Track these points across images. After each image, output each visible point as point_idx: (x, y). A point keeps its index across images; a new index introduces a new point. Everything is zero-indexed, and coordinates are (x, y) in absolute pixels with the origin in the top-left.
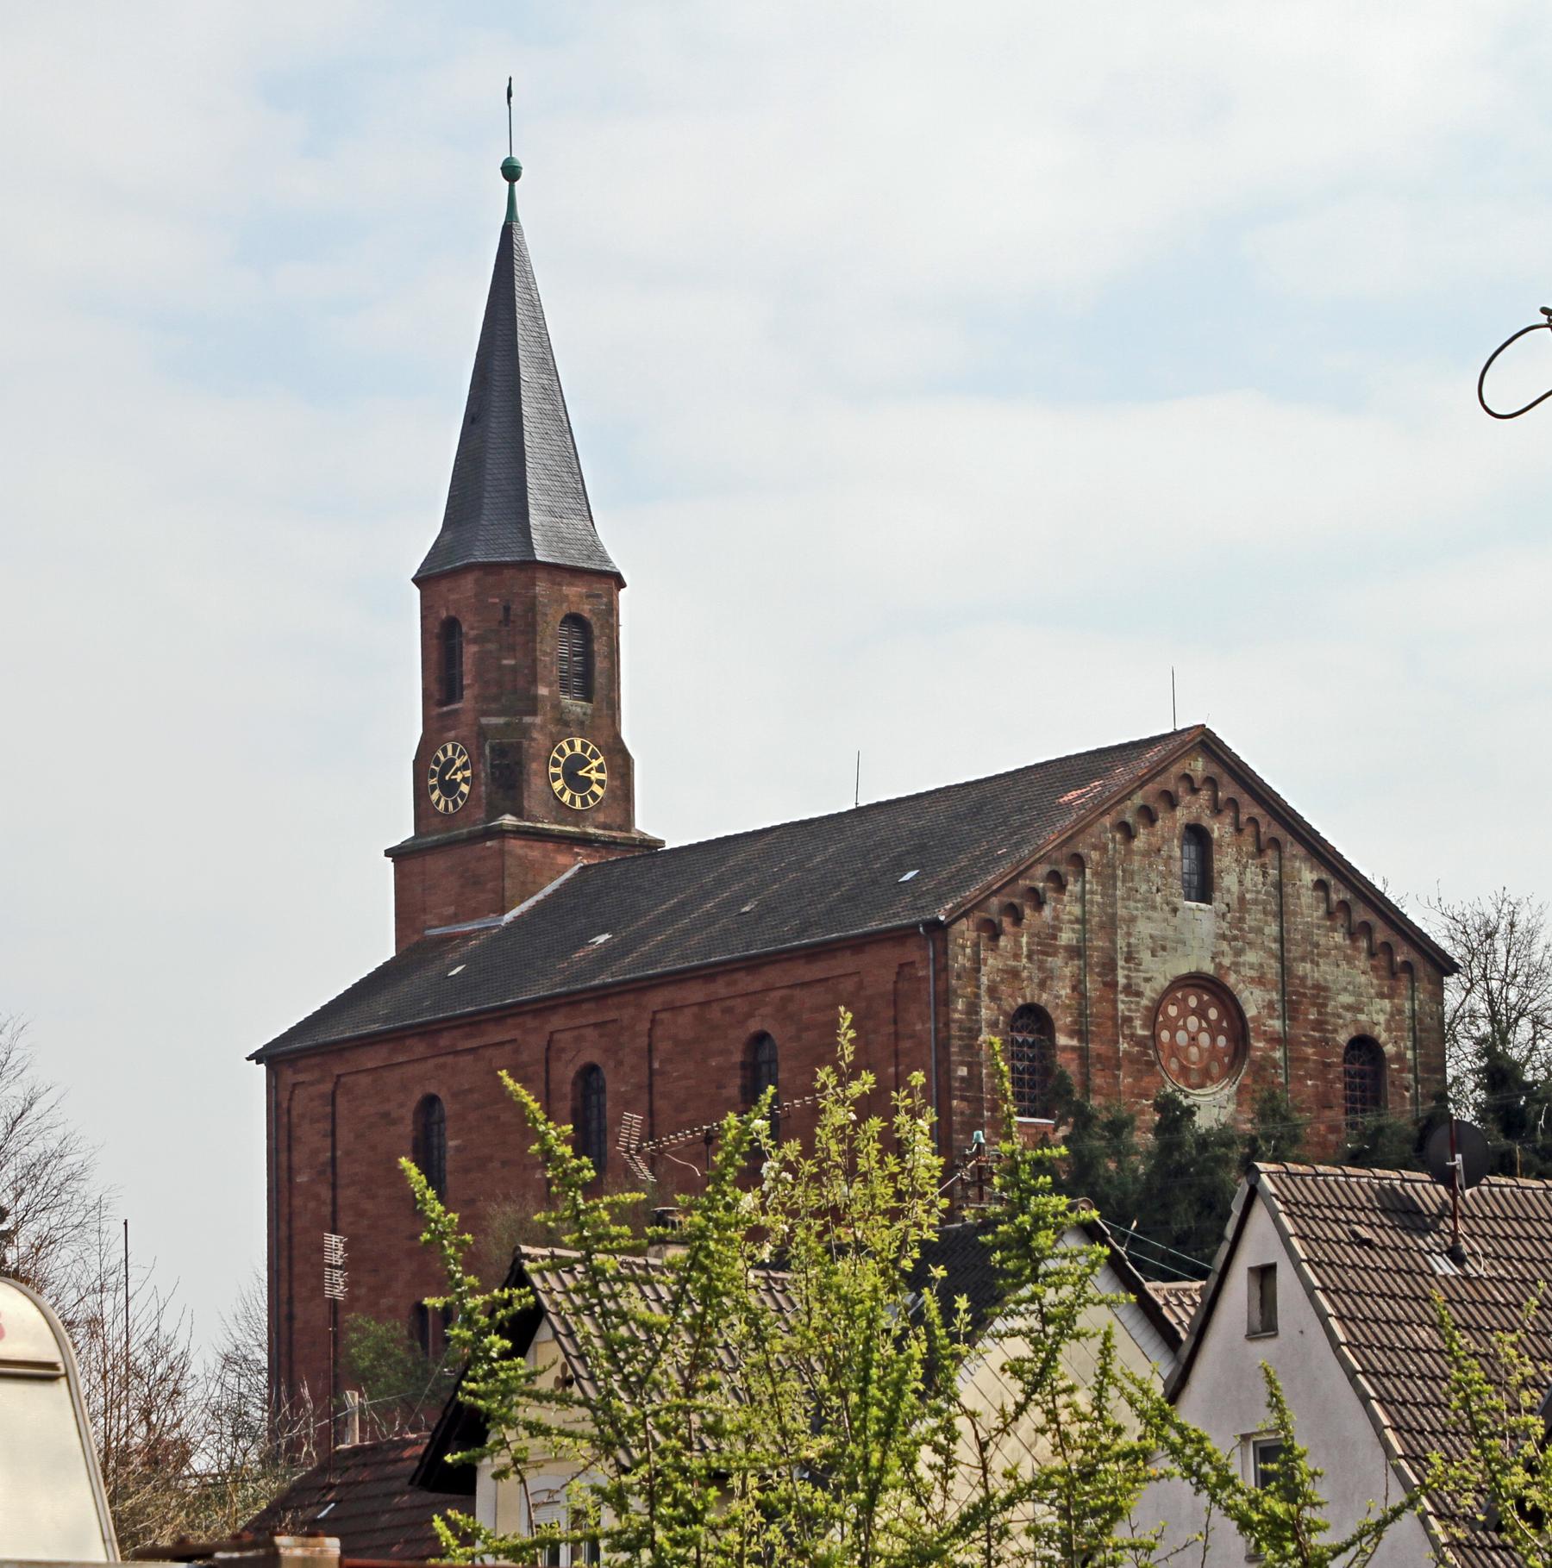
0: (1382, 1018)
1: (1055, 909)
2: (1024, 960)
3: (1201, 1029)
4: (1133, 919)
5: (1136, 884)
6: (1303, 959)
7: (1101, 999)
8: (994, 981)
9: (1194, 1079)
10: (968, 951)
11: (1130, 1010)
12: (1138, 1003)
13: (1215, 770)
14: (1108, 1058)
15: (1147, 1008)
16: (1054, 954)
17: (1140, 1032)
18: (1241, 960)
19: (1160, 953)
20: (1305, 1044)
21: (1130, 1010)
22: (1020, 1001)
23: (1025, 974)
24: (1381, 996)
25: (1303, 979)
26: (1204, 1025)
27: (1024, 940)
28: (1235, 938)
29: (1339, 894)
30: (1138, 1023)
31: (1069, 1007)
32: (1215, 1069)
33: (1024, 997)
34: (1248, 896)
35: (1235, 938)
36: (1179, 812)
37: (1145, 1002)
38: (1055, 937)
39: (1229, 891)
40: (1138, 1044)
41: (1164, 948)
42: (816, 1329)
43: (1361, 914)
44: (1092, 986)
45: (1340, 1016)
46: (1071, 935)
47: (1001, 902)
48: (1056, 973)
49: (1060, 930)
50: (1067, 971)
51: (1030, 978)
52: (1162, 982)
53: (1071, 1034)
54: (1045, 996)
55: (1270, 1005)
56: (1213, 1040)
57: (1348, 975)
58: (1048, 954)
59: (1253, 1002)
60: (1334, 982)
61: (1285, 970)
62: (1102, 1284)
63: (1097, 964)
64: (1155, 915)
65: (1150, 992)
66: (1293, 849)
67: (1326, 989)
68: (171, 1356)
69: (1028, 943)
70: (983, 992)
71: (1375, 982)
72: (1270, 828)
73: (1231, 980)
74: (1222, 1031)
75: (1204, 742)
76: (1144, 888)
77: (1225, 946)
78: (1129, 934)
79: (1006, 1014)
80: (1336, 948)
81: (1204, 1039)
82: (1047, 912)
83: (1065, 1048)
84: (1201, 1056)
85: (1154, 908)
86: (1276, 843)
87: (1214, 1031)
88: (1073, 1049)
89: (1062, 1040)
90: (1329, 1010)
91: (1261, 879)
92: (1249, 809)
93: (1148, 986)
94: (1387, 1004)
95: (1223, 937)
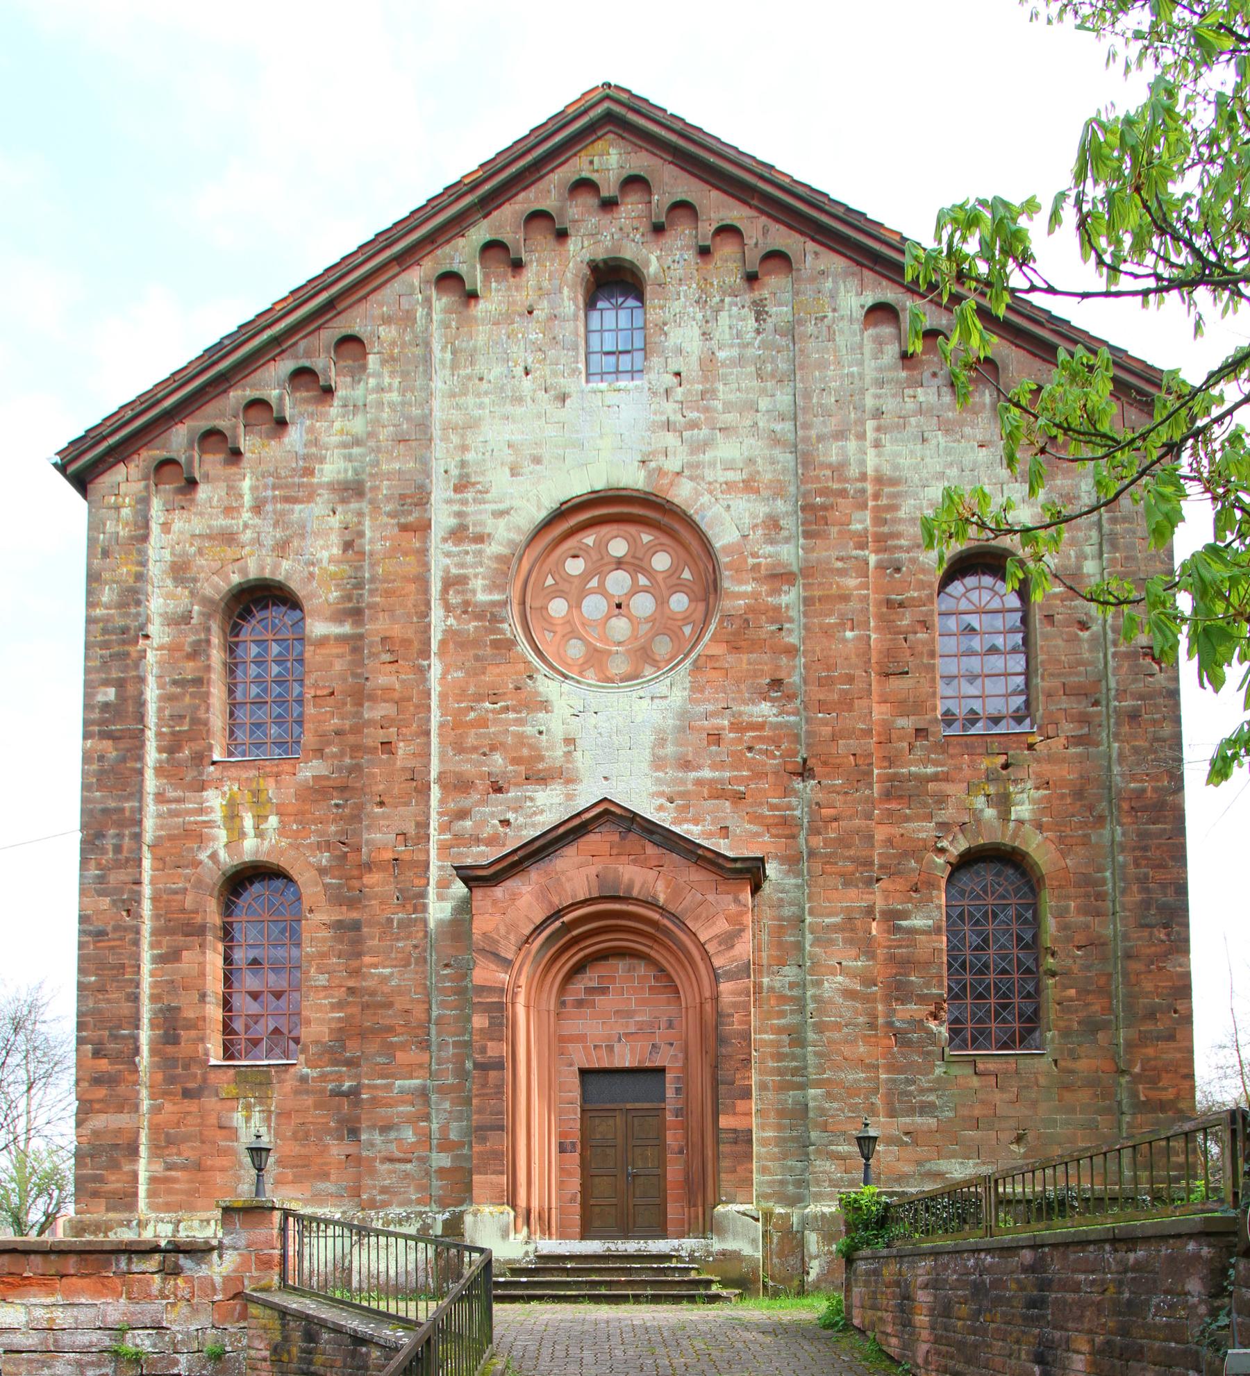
2: (246, 515)
4: (472, 425)
5: (480, 368)
6: (840, 435)
7: (392, 553)
9: (619, 666)
10: (125, 512)
11: (462, 565)
12: (480, 553)
13: (642, 162)
14: (406, 642)
15: (500, 558)
16: (310, 498)
17: (482, 597)
18: (707, 457)
19: (528, 467)
20: (842, 573)
21: (462, 565)
22: (236, 579)
23: (248, 536)
26: (594, 583)
27: (246, 485)
28: (694, 425)
30: (478, 584)
33: (243, 571)
35: (694, 425)
36: (572, 245)
38: (309, 472)
39: (680, 351)
40: (479, 616)
41: (537, 460)
44: (375, 537)
46: (342, 464)
48: (313, 526)
49: (322, 460)
51: (258, 541)
52: (535, 498)
53: (339, 616)
54: (286, 565)
55: (773, 524)
56: (662, 602)
57: (948, 452)
59: (728, 522)
60: (916, 468)
63: (388, 499)
64: (519, 410)
65: (505, 534)
66: (815, 259)
68: (1081, 707)
69: (254, 489)
72: (763, 233)
73: (682, 494)
75: (613, 115)
76: (498, 370)
77: (671, 439)
79: (205, 601)
80: (920, 411)
81: (643, 605)
82: (294, 436)
83: (323, 641)
85: (519, 400)
86: (778, 258)
87: (662, 589)
90: (901, 514)
91: (752, 323)
92: (718, 208)
93: (502, 522)
95: (668, 426)
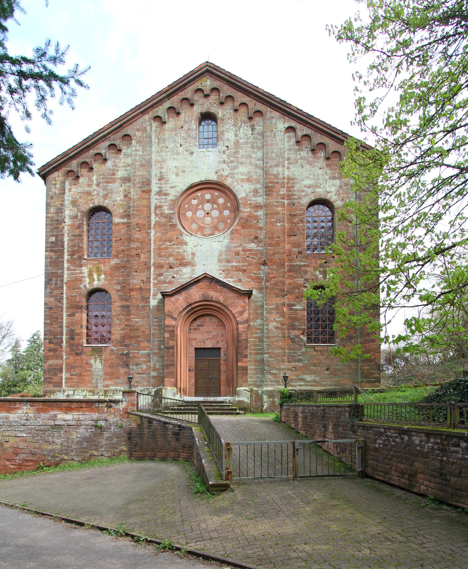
0: (333, 189)
1: (114, 162)
2: (94, 187)
3: (203, 209)
4: (164, 161)
5: (167, 144)
6: (277, 166)
8: (76, 198)
9: (207, 231)
11: (161, 202)
12: (166, 199)
15: (172, 200)
16: (114, 182)
17: (167, 212)
19: (181, 174)
20: (277, 206)
21: (161, 202)
22: (91, 205)
24: (334, 178)
25: (276, 176)
26: (200, 207)
27: (95, 178)
28: (232, 162)
29: (302, 130)
30: (165, 208)
31: (121, 205)
32: (221, 226)
33: (94, 203)
34: (241, 141)
35: (232, 162)
36: (195, 108)
37: (170, 198)
38: (114, 174)
39: (228, 140)
40: (166, 217)
41: (184, 172)
42: (399, 206)
43: (318, 138)
45: (303, 191)
46: (124, 172)
47: (78, 163)
49: (118, 171)
50: (122, 189)
51: (98, 194)
53: (123, 217)
54: (107, 201)
56: (221, 213)
58: (110, 183)
61: (266, 173)
62: (338, 317)
65: (173, 194)
66: (270, 113)
67: (293, 179)
69: (97, 179)
70: (67, 203)
71: (329, 172)
72: (254, 105)
74: (226, 208)
75: (209, 70)
76: (171, 145)
78: (161, 168)
79: (82, 212)
82: (109, 164)
83: (118, 224)
84: (213, 220)
86: (259, 112)
88: (124, 223)
89: (117, 220)
91: (250, 132)
93: (173, 190)
94: (337, 182)
